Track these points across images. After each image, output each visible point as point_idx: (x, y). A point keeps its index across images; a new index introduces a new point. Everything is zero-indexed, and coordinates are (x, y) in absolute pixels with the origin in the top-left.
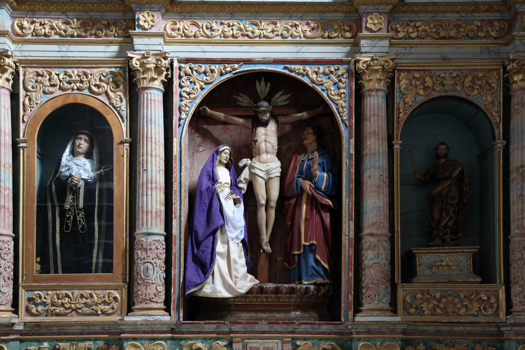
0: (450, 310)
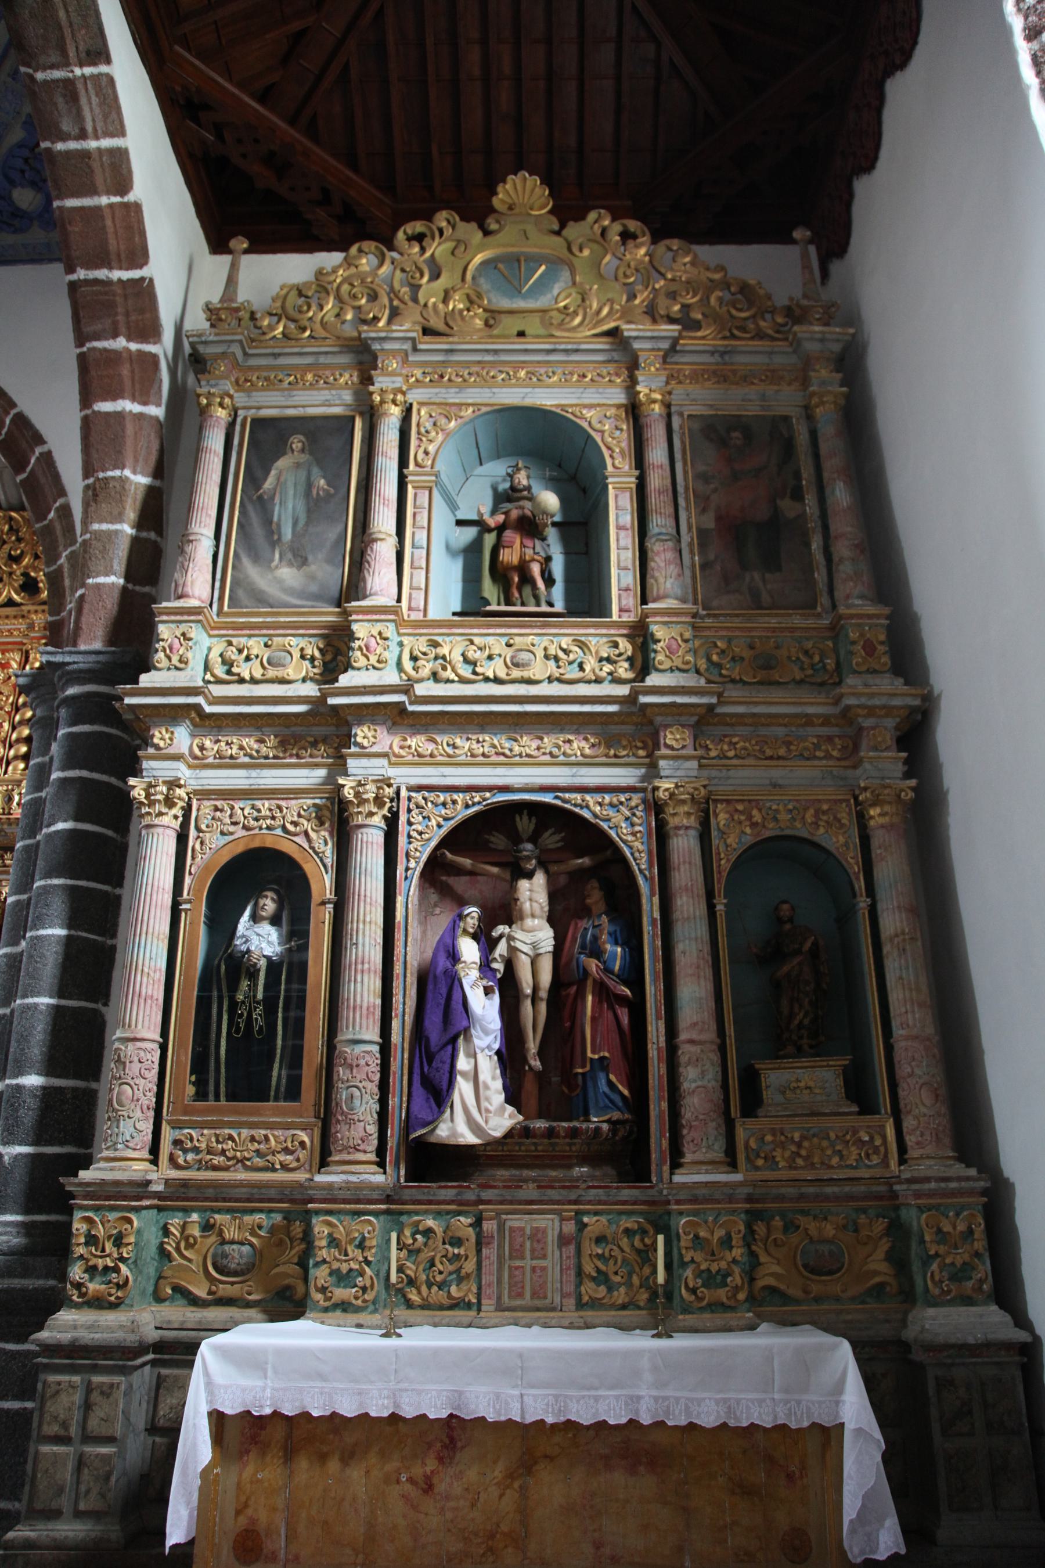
0: (816, 1160)
